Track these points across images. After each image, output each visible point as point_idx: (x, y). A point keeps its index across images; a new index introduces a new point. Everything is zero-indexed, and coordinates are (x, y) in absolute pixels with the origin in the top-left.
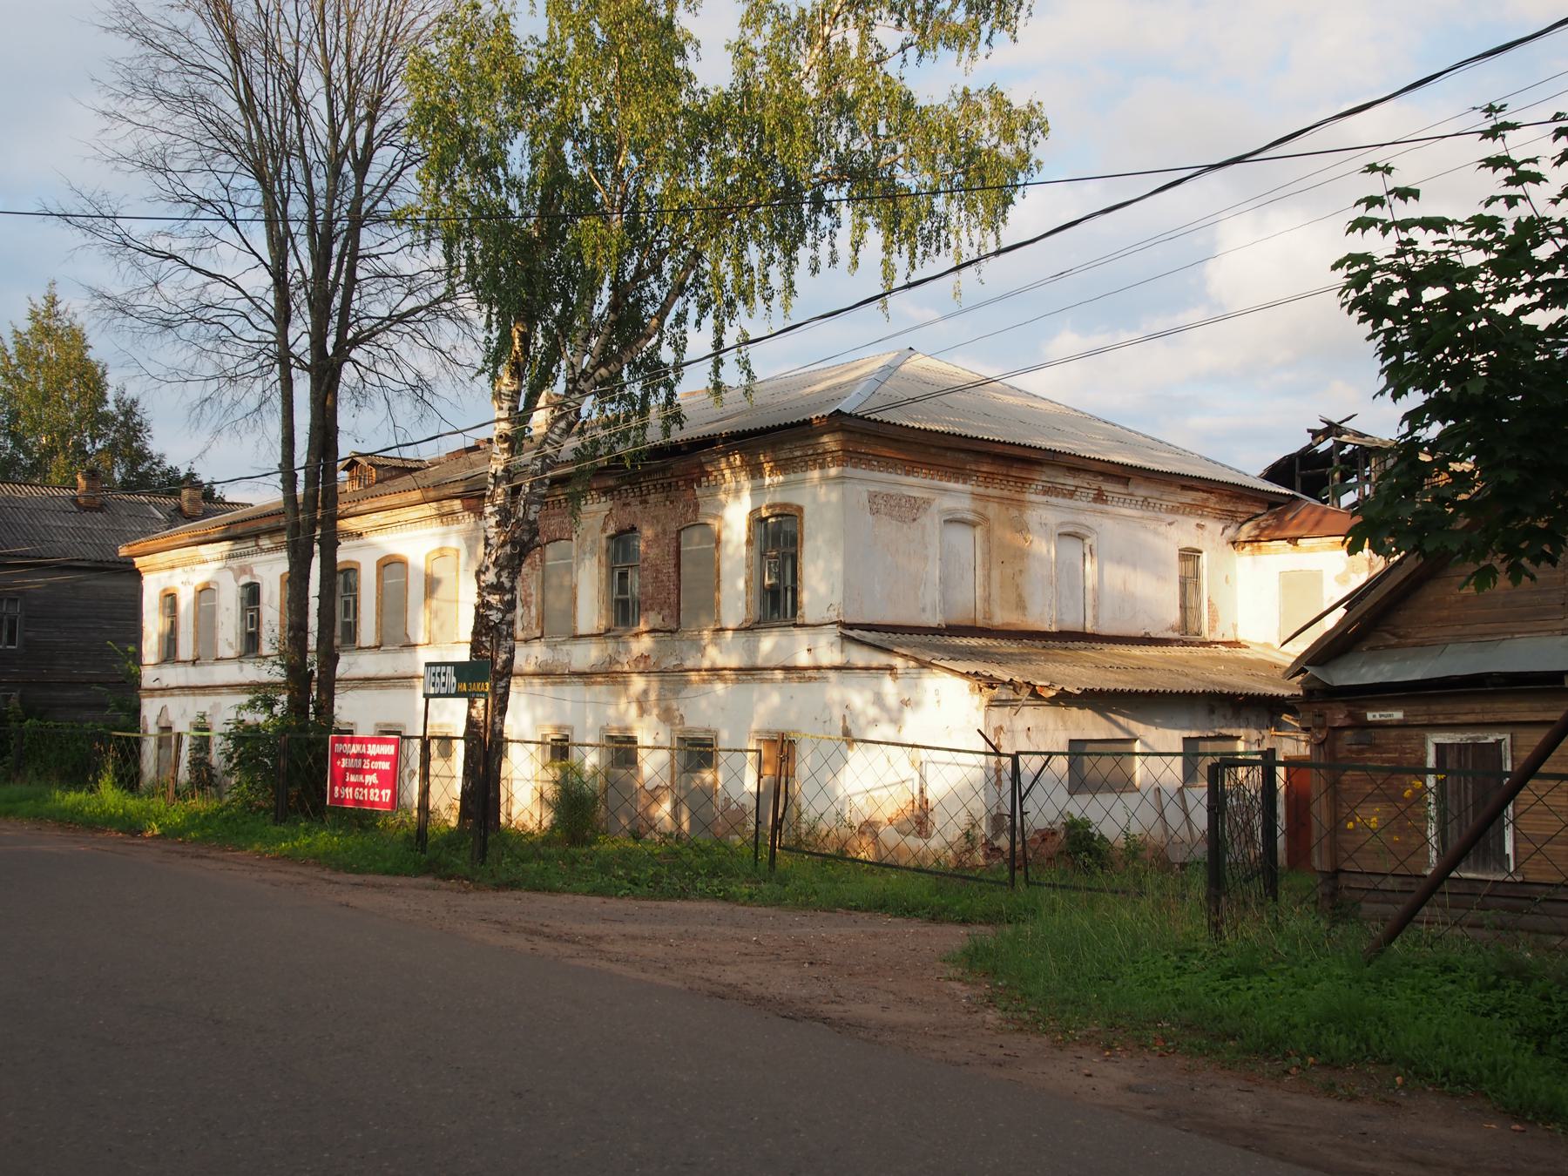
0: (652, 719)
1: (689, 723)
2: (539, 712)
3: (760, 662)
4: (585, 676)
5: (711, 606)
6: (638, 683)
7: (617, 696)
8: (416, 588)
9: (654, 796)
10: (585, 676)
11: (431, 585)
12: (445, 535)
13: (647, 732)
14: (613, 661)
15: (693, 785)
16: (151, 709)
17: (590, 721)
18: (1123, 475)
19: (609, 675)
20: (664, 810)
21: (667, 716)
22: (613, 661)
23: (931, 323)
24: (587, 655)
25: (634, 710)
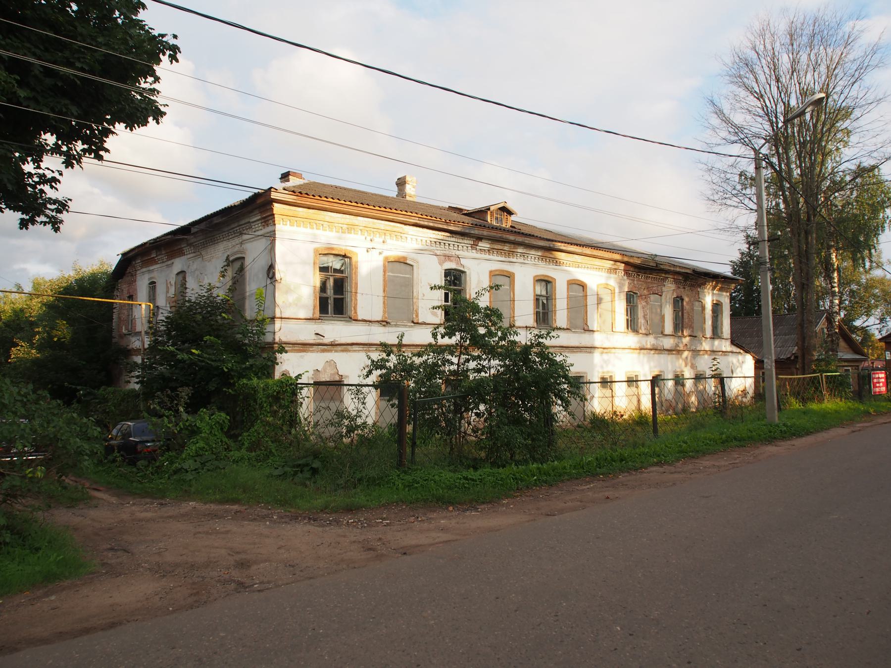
0: (689, 367)
1: (699, 369)
2: (652, 364)
3: (715, 349)
4: (670, 351)
5: (703, 330)
6: (686, 354)
7: (678, 359)
8: (591, 301)
9: (689, 395)
10: (670, 351)
11: (599, 301)
12: (609, 278)
13: (688, 373)
14: (677, 345)
15: (858, 323)
16: (290, 365)
17: (670, 368)
18: (370, 322)
19: (675, 351)
20: (693, 399)
21: (693, 366)
22: (677, 345)
23: (179, 101)
24: (668, 343)
25: (683, 364)
